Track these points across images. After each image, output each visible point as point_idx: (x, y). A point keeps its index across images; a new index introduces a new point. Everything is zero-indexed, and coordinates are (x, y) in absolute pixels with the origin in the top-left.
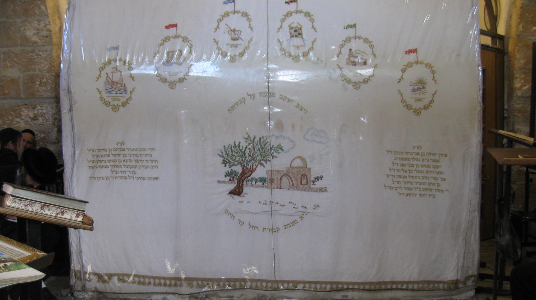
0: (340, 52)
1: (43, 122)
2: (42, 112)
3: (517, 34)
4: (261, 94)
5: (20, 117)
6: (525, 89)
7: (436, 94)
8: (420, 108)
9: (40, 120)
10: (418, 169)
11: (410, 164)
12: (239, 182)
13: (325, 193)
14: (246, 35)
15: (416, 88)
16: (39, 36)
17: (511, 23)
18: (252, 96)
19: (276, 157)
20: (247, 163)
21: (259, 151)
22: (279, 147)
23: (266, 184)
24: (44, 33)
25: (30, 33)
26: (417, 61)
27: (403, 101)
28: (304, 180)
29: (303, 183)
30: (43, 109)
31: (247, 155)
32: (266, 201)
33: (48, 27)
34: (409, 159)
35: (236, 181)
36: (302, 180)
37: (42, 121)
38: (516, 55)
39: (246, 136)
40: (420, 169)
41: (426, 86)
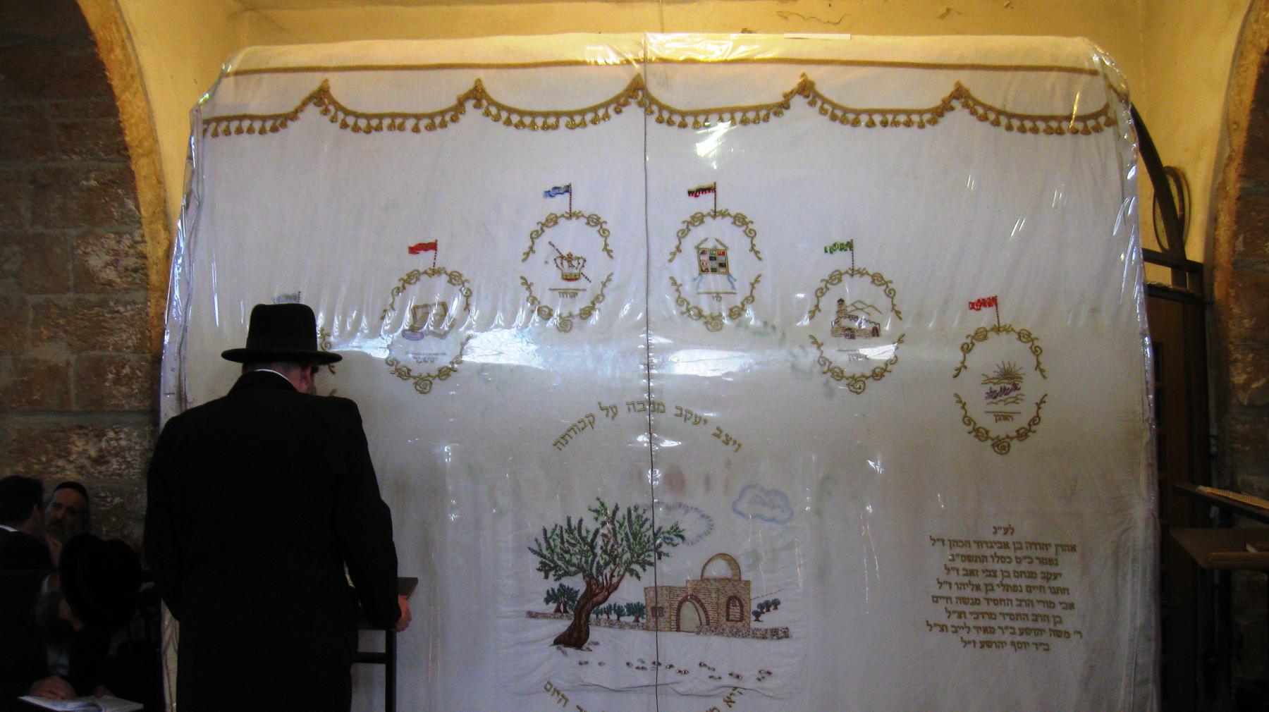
0: (817, 306)
1: (120, 469)
2: (119, 444)
3: (1233, 259)
4: (631, 407)
5: (65, 457)
6: (1257, 388)
7: (1045, 402)
8: (1008, 437)
9: (113, 465)
10: (1006, 581)
11: (987, 571)
12: (578, 616)
13: (784, 641)
14: (596, 268)
15: (997, 388)
16: (119, 269)
17: (1216, 233)
18: (612, 411)
19: (667, 555)
20: (597, 569)
21: (628, 540)
22: (675, 531)
23: (644, 621)
24: (131, 262)
25: (95, 261)
26: (997, 324)
27: (967, 420)
28: (735, 611)
29: (731, 617)
30: (120, 439)
31: (598, 551)
32: (643, 662)
33: (140, 247)
34: (986, 557)
35: (572, 613)
36: (731, 610)
37: (118, 467)
38: (1231, 309)
39: (597, 505)
40: (1012, 581)
41: (1020, 385)
